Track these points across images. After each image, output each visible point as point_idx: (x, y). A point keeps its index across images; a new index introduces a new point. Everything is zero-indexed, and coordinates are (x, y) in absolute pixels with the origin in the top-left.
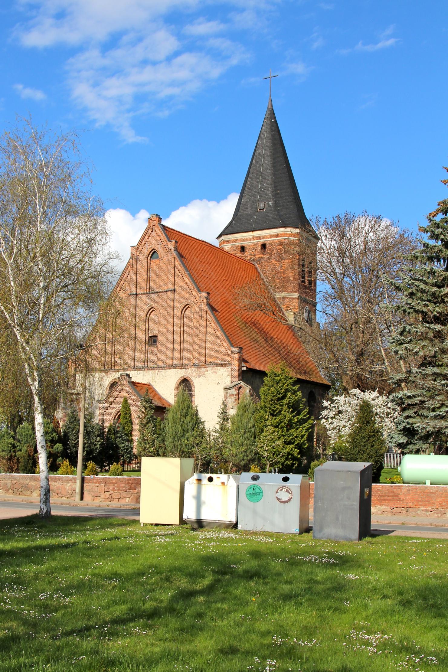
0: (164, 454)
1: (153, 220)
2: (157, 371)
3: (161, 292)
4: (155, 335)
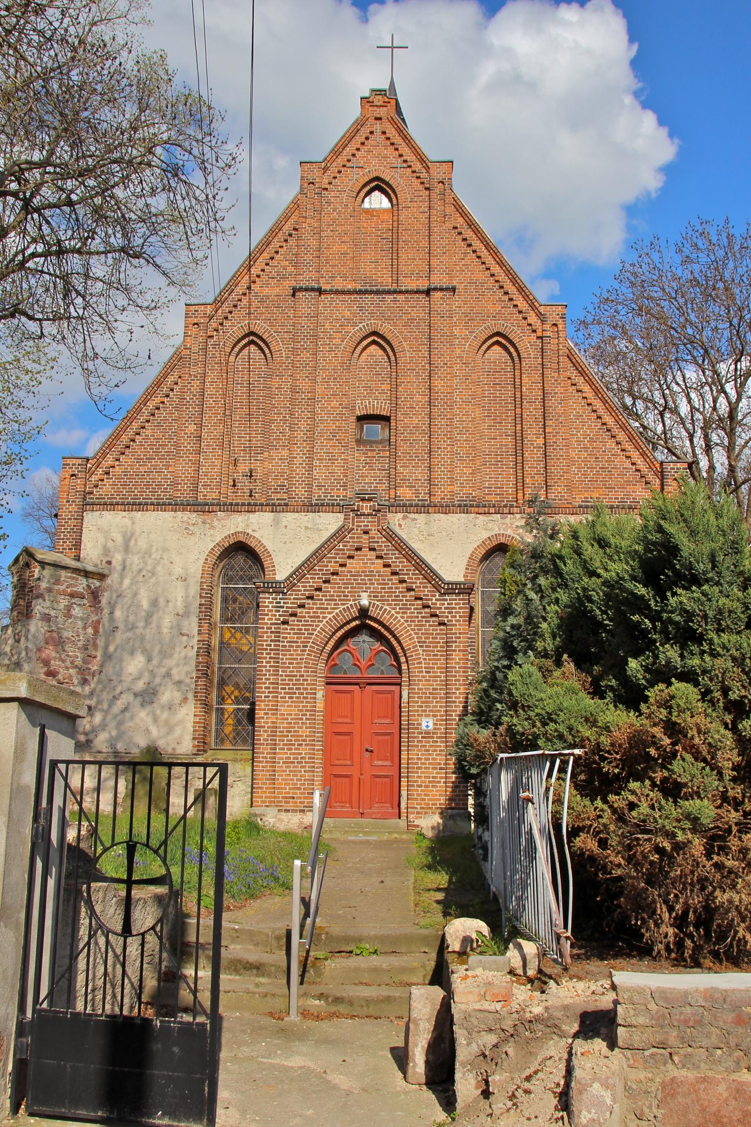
0: (532, 501)
1: (376, 103)
2: (400, 515)
3: (407, 292)
4: (384, 413)
